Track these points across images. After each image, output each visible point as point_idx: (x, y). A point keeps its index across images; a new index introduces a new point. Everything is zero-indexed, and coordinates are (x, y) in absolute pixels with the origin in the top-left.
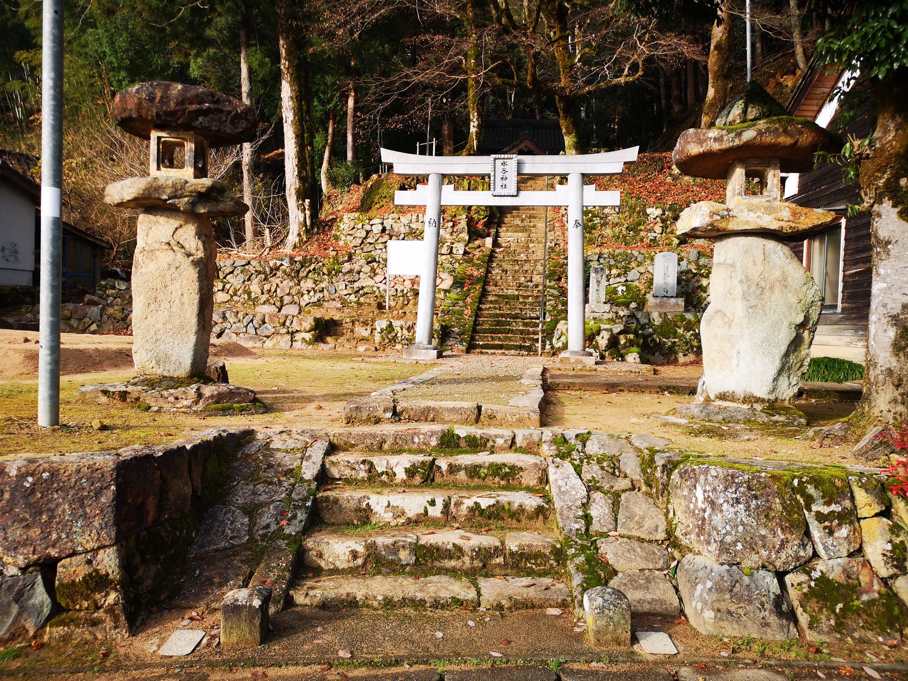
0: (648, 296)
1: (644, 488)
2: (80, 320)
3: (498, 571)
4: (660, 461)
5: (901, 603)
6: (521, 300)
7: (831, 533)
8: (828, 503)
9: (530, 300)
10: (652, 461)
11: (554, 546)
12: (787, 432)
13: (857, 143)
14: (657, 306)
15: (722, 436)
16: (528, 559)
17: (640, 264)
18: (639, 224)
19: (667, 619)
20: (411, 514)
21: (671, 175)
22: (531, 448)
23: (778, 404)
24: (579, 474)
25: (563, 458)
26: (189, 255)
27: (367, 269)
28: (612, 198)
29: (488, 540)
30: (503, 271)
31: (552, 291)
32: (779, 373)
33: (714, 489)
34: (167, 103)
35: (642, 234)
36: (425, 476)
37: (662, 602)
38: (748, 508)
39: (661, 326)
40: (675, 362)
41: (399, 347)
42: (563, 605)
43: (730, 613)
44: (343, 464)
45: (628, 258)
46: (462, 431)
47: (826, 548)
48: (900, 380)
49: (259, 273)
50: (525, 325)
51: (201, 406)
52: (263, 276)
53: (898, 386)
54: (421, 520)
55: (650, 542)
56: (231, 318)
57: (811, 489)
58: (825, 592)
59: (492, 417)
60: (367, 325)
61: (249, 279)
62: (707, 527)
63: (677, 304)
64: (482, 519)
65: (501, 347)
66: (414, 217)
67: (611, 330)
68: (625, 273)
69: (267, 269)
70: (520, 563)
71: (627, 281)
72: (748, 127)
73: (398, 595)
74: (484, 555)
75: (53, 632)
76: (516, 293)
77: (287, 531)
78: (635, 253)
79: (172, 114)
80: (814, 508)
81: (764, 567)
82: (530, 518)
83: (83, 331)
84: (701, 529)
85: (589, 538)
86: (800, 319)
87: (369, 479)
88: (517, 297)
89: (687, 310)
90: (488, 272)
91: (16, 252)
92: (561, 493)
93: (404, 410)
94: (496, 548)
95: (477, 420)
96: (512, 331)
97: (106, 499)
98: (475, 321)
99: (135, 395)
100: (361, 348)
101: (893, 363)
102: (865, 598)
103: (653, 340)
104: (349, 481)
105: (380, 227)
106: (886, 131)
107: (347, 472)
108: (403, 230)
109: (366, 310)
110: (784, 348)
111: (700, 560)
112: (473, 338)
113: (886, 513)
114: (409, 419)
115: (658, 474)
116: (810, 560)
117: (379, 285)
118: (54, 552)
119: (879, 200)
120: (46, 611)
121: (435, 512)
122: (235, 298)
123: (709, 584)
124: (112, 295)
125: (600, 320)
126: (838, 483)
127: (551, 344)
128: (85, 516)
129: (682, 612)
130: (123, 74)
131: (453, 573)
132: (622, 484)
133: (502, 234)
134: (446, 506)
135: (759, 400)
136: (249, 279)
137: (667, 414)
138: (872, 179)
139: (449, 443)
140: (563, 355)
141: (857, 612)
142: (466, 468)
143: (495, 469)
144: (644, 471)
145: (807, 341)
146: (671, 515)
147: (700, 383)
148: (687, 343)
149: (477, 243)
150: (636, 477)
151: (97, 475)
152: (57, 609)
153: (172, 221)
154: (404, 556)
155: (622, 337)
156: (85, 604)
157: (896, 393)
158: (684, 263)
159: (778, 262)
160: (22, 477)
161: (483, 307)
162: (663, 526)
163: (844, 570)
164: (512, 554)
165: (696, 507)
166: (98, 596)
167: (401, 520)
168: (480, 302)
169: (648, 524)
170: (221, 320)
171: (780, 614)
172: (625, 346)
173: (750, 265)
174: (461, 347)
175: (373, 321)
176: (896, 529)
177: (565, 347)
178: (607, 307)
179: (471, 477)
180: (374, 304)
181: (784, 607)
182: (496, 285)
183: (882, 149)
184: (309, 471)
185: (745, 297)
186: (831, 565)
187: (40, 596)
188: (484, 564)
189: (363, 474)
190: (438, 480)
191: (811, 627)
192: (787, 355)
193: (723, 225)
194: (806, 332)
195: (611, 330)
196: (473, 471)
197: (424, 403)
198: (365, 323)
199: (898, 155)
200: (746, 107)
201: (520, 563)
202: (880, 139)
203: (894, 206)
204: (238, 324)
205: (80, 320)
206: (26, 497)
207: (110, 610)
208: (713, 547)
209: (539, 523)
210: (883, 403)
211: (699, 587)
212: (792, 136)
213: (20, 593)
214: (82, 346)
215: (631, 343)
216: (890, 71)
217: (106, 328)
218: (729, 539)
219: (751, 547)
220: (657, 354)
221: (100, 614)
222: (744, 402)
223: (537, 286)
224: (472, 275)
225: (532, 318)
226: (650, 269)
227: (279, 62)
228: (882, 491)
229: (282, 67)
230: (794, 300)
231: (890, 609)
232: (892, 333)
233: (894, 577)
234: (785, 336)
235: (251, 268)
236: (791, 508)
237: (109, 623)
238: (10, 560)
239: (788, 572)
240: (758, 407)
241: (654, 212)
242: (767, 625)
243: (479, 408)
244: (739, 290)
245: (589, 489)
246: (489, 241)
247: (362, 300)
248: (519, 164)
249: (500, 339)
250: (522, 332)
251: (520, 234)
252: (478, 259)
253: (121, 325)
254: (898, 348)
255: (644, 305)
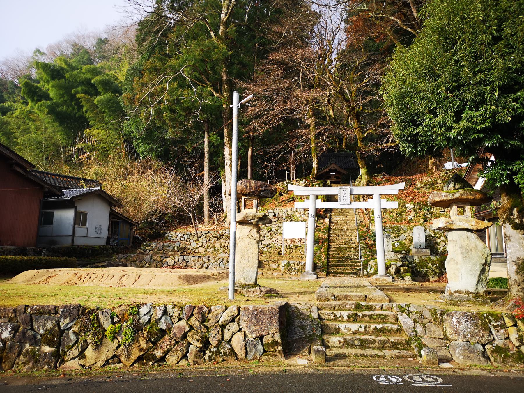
0: (410, 248)
1: (433, 322)
2: (141, 262)
3: (387, 348)
4: (438, 312)
5: (522, 354)
6: (348, 250)
7: (498, 331)
8: (496, 322)
9: (352, 250)
10: (436, 312)
11: (406, 340)
12: (483, 304)
13: (495, 203)
14: (416, 253)
15: (459, 305)
16: (398, 344)
17: (405, 232)
18: (403, 212)
19: (450, 360)
20: (354, 330)
21: (416, 188)
22: (389, 309)
23: (479, 294)
24: (410, 317)
25: (402, 312)
26: (255, 239)
27: (268, 234)
28: (394, 205)
29: (383, 338)
30: (336, 235)
31: (363, 245)
32: (478, 282)
33: (459, 318)
34: (252, 189)
35: (405, 217)
36: (354, 318)
37: (446, 356)
38: (471, 323)
39: (420, 263)
40: (428, 280)
41: (293, 273)
42: (413, 357)
43: (468, 357)
44: (325, 314)
45: (399, 229)
46: (363, 303)
47: (497, 336)
48: (519, 283)
49: (214, 237)
50: (352, 262)
51: (262, 295)
52: (216, 239)
53: (519, 286)
54: (357, 332)
55: (439, 339)
56: (212, 260)
57: (490, 317)
58: (498, 350)
59: (371, 299)
60: (275, 262)
61: (209, 240)
62: (458, 331)
63: (426, 252)
64: (382, 331)
65: (342, 273)
66: (289, 209)
67: (396, 265)
68: (398, 236)
69: (218, 235)
70: (394, 346)
71: (399, 240)
72: (457, 192)
73: (359, 353)
74: (383, 343)
75: (264, 358)
76: (345, 246)
77: (316, 334)
78: (403, 227)
79: (253, 192)
80: (492, 323)
81: (478, 343)
82: (395, 332)
83: (142, 267)
84: (456, 332)
85: (417, 338)
86: (484, 262)
87: (335, 319)
88: (346, 248)
89: (431, 255)
90: (329, 236)
91: (101, 229)
92: (404, 323)
93: (338, 296)
94: (387, 341)
95: (365, 300)
96: (346, 265)
97: (277, 317)
98: (328, 260)
99: (239, 291)
100: (275, 274)
101: (516, 278)
102: (511, 352)
103: (416, 270)
104: (328, 320)
105: (273, 214)
106: (504, 200)
107: (327, 317)
108: (284, 215)
109: (273, 255)
110: (479, 273)
111: (456, 342)
112: (328, 269)
113: (515, 325)
114: (340, 299)
115: (438, 316)
116: (492, 341)
117: (275, 242)
118: (263, 333)
119: (504, 222)
120: (262, 351)
121: (362, 330)
122: (208, 250)
123: (460, 348)
124: (149, 249)
125: (390, 260)
126: (499, 315)
127: (367, 271)
128: (271, 323)
129: (452, 359)
130: (140, 141)
131: (373, 348)
132: (425, 321)
133: (333, 217)
134: (365, 327)
135: (471, 293)
136: (209, 240)
137: (435, 299)
138: (502, 216)
139: (359, 307)
140: (374, 277)
141: (509, 357)
142: (368, 316)
143: (379, 316)
144: (433, 316)
145: (487, 270)
146: (445, 329)
147: (447, 288)
148: (433, 271)
149: (321, 221)
150: (430, 318)
151: (274, 310)
152: (264, 351)
153: (249, 227)
154: (356, 342)
155: (402, 268)
156: (272, 350)
157: (519, 288)
158: (427, 231)
159: (473, 240)
160: (254, 311)
161: (330, 253)
162: (442, 334)
163: (504, 344)
164: (392, 343)
165: (453, 325)
166: (276, 347)
167: (350, 332)
168: (328, 251)
169: (437, 333)
170: (207, 261)
171: (485, 357)
172: (403, 273)
173: (462, 241)
174: (323, 273)
175: (278, 260)
176: (519, 330)
177: (376, 272)
178: (393, 254)
179: (370, 319)
180: (277, 252)
181: (486, 355)
182: (334, 242)
183: (503, 206)
184: (315, 316)
185: (462, 253)
186: (499, 342)
187: (260, 347)
188: (383, 346)
189: (332, 317)
190: (359, 320)
191: (495, 361)
192: (480, 275)
193: (450, 227)
194: (487, 267)
195: (396, 265)
196: (371, 317)
197: (345, 294)
198: (274, 262)
199: (508, 208)
200: (455, 184)
201: (394, 346)
202: (502, 202)
203: (510, 225)
204: (215, 263)
205: (141, 262)
206: (255, 317)
207: (279, 352)
208: (461, 336)
209: (398, 334)
210: (515, 292)
211: (457, 350)
212: (473, 196)
213: (255, 346)
214: (190, 274)
215: (406, 271)
216: (501, 185)
217: (153, 265)
218: (465, 333)
219: (473, 336)
220: (419, 276)
221: (276, 353)
222: (465, 294)
223: (354, 243)
224: (322, 238)
225: (355, 259)
226: (410, 234)
227: (224, 138)
228: (513, 318)
229: (225, 141)
230: (481, 255)
231: (520, 356)
232: (515, 267)
233: (520, 346)
234: (479, 268)
235: (210, 235)
236: (484, 323)
237: (279, 356)
238: (250, 336)
239: (486, 345)
240: (471, 295)
241: (409, 206)
242: (480, 360)
243: (366, 296)
244: (459, 251)
245: (414, 322)
246: (327, 220)
247: (270, 250)
248: (351, 190)
249: (341, 269)
250: (351, 266)
251: (342, 216)
252: (323, 229)
253: (160, 264)
254: (517, 273)
255: (409, 252)
